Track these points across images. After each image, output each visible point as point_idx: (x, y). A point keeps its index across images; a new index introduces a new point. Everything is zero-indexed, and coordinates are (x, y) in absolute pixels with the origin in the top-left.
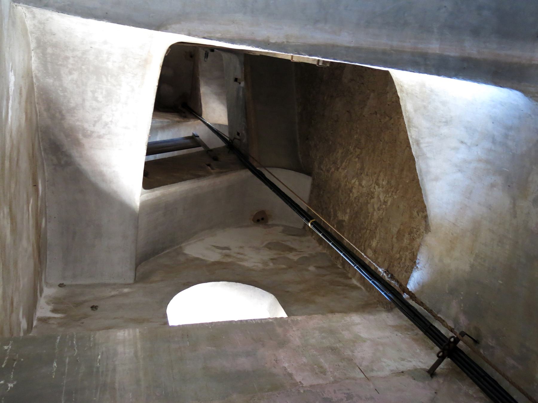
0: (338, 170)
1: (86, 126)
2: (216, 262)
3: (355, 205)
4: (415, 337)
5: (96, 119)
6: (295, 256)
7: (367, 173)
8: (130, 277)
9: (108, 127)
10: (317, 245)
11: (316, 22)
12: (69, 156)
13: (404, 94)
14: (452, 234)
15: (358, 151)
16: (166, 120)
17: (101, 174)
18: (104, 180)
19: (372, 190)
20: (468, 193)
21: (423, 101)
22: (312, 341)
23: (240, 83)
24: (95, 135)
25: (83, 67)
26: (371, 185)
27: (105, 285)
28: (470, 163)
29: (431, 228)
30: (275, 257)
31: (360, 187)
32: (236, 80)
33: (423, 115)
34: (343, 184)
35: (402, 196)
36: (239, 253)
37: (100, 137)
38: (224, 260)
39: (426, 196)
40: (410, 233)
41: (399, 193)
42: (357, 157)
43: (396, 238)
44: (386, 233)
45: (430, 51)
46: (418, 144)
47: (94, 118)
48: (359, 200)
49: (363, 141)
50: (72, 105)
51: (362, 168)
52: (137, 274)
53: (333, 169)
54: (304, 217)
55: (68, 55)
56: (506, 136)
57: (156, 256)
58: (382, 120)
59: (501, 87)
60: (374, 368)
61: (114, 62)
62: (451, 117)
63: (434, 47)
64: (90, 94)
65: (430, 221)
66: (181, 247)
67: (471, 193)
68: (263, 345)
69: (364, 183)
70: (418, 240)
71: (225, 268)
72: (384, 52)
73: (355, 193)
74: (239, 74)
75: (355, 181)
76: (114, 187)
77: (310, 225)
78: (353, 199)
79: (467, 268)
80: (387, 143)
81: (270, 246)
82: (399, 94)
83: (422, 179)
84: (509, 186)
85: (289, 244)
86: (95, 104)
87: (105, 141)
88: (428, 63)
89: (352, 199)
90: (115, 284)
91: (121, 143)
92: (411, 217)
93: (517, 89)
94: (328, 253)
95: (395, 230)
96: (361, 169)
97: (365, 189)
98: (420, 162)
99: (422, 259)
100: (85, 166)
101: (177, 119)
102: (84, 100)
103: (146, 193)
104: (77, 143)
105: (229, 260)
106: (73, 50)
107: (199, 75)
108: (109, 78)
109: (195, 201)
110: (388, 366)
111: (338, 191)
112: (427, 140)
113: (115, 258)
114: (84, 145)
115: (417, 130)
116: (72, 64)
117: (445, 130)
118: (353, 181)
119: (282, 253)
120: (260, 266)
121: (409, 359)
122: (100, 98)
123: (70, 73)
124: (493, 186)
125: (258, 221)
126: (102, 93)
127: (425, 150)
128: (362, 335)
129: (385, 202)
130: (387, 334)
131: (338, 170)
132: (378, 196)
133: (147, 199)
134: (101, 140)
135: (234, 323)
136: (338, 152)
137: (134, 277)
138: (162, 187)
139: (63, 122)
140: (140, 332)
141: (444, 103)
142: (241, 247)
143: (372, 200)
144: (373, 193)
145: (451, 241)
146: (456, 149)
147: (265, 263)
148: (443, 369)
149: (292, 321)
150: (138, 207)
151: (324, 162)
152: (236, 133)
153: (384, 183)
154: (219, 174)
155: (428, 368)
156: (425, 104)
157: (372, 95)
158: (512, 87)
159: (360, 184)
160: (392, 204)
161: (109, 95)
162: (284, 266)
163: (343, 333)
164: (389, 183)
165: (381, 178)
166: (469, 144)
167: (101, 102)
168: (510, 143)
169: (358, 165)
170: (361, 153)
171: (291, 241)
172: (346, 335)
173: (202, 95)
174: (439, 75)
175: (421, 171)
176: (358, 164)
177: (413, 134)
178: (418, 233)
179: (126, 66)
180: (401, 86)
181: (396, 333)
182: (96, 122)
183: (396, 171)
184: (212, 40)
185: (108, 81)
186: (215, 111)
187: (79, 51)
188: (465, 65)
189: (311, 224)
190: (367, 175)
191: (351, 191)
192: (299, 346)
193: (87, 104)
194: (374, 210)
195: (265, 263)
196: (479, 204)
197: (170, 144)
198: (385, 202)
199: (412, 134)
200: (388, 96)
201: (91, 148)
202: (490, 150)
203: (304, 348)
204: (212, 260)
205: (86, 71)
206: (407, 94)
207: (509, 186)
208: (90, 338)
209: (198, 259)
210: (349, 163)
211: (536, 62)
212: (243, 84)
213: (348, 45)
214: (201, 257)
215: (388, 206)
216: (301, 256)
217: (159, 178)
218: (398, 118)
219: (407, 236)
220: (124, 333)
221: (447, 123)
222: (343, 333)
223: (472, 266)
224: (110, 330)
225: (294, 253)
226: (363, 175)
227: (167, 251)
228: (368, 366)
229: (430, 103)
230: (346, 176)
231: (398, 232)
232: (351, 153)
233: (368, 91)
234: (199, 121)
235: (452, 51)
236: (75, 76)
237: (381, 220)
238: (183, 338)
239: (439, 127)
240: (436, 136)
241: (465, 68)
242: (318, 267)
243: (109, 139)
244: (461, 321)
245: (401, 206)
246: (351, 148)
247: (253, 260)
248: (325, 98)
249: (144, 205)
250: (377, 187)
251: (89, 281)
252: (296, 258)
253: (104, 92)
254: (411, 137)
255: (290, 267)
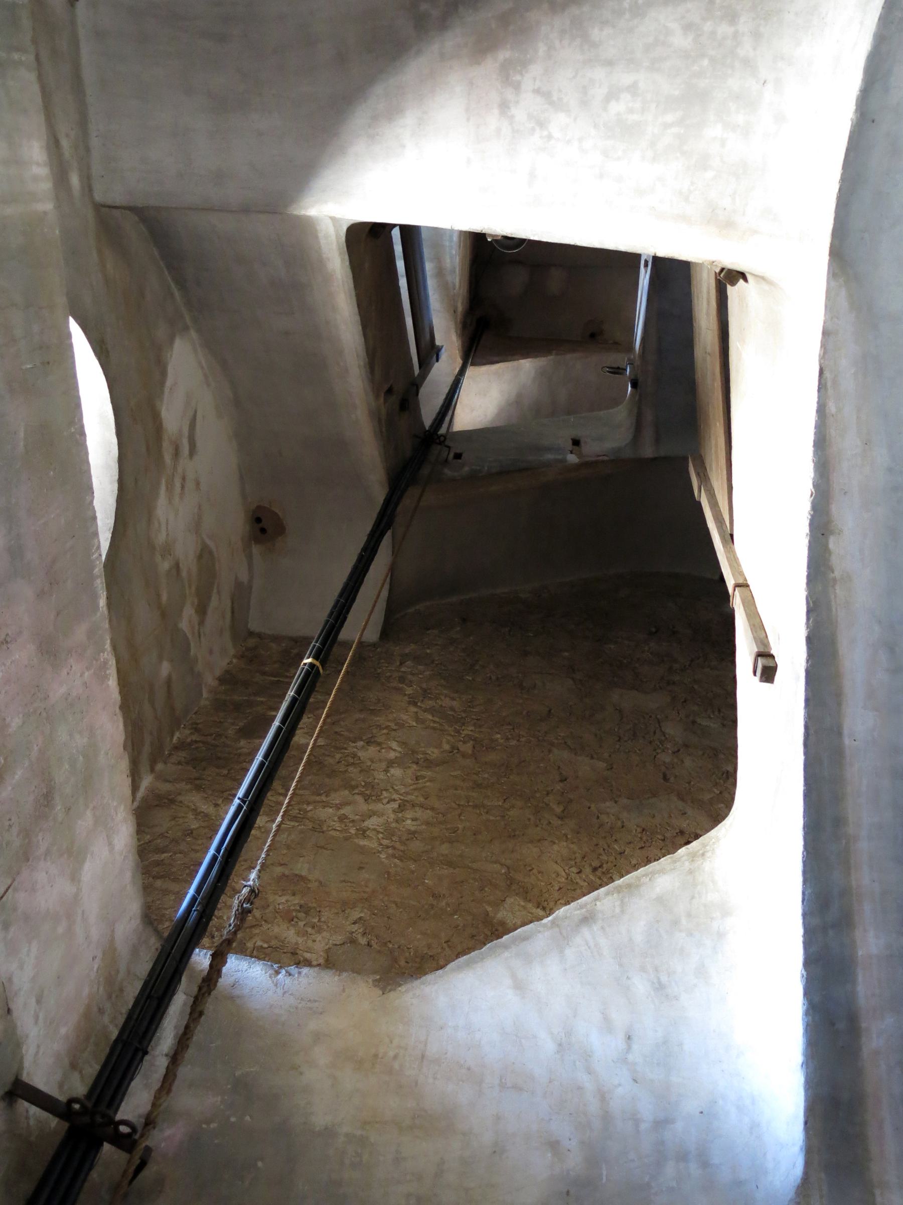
0: (409, 703)
1: (535, 69)
2: (161, 424)
3: (338, 756)
4: (95, 1009)
5: (555, 98)
6: (190, 622)
7: (423, 777)
8: (112, 192)
9: (533, 130)
10: (218, 673)
11: (891, 649)
12: (443, 24)
13: (687, 864)
14: (396, 1057)
15: (467, 748)
16: (457, 281)
17: (393, 113)
18: (375, 118)
19: (385, 794)
20: (514, 1082)
21: (689, 915)
22: (62, 734)
23: (571, 452)
24: (509, 94)
25: (706, 62)
26: (397, 791)
27: (83, 123)
28: (589, 1071)
29: (392, 995)
30: (184, 574)
31: (384, 765)
32: (576, 442)
33: (658, 922)
34: (381, 720)
35: (388, 873)
36: (184, 479)
37: (504, 106)
38: (166, 444)
39: (468, 964)
40: (305, 909)
41: (396, 866)
42: (453, 748)
43: (284, 875)
44: (288, 847)
45: (858, 934)
46: (587, 919)
47: (560, 91)
48: (353, 764)
49: (492, 757)
50: (596, 33)
51: (429, 764)
52: (114, 211)
53: (409, 691)
54: (323, 644)
55: (742, 19)
56: (682, 1157)
57: (162, 264)
58: (551, 797)
59: (806, 1123)
60: (12, 929)
61: (723, 143)
62: (676, 998)
63: (870, 942)
64: (627, 79)
65: (409, 986)
66: (186, 328)
67: (517, 1088)
68: (41, 595)
69: (396, 772)
70: (292, 932)
71: (148, 449)
72: (839, 822)
73: (367, 754)
74: (592, 449)
75: (395, 750)
76: (359, 147)
77: (308, 661)
78: (351, 750)
79: (320, 1120)
80: (503, 817)
81: (205, 555)
82: (682, 851)
83: (506, 947)
84: (568, 1193)
85: (214, 602)
86: (599, 92)
87: (493, 120)
88: (831, 933)
89: (351, 747)
90: (88, 150)
91: (449, 163)
92: (345, 906)
93: (808, 1164)
94: (203, 703)
95: (301, 867)
96: (426, 760)
97: (382, 776)
98: (547, 934)
99: (304, 982)
100: (414, 69)
101: (460, 308)
102: (610, 63)
103: (337, 231)
104: (483, 46)
105: (168, 458)
106: (757, 36)
107: (557, 354)
108: (675, 130)
109: (311, 360)
110: (21, 967)
111: (361, 711)
112: (602, 941)
113: (165, 152)
114: (479, 64)
115: (618, 910)
116: (713, 33)
117: (640, 986)
118: (394, 745)
119: (193, 588)
120: (161, 538)
121: (41, 1016)
122: (615, 108)
123: (688, 27)
124: (554, 1145)
125: (258, 520)
126: (631, 111)
127: (578, 940)
128: (87, 866)
129: (363, 833)
130: (95, 933)
131: (409, 703)
132: (372, 814)
133: (321, 235)
134: (496, 111)
135: (88, 498)
136: (453, 699)
137: (109, 202)
138: (351, 276)
139: (545, 6)
140: (45, 213)
141: (701, 971)
142: (198, 484)
143: (359, 799)
144: (379, 800)
145: (376, 1056)
146: (607, 1025)
147: (167, 550)
148: (27, 1118)
149: (106, 663)
150: (303, 212)
151: (421, 667)
152: (458, 451)
153: (409, 822)
154: (375, 415)
155: (25, 1078)
156: (684, 921)
157: (602, 765)
158: (809, 1151)
159: (391, 763)
160: (362, 850)
161: (625, 130)
162: (164, 598)
163: (89, 813)
164: (413, 834)
165: (419, 813)
166: (630, 1057)
167: (605, 109)
168: (670, 1170)
169: (434, 753)
170: (464, 756)
171: (220, 603)
172: (85, 823)
173: (515, 363)
174: (807, 963)
175: (525, 938)
176: (436, 751)
177: (605, 901)
178: (310, 930)
179: (710, 174)
180: (703, 855)
181: (100, 955)
182: (546, 95)
183: (445, 849)
184: (819, 390)
185: (666, 126)
186: (484, 397)
187: (755, 49)
188: (841, 1025)
189: (311, 665)
190: (417, 778)
191: (369, 743)
192: (47, 698)
193: (599, 73)
194: (338, 807)
195: (167, 550)
196: (498, 1118)
197: (422, 293)
198: (363, 833)
199: (603, 900)
200: (608, 804)
201: (471, 84)
202: (637, 1121)
203: (44, 714)
204: (164, 414)
205: (696, 68)
206: (691, 872)
207: (568, 1193)
208: (17, 49)
209: (164, 374)
210: (434, 728)
211: (879, 1199)
212: (572, 459)
213: (846, 731)
214: (169, 383)
215: (356, 840)
216: (190, 637)
217: (367, 265)
218: (566, 835)
219: (296, 900)
220: (38, 164)
221: (659, 987)
222: (89, 813)
223: (329, 1133)
224: (42, 118)
225: (195, 619)
226: (415, 766)
227: (177, 294)
228: (15, 909)
229: (690, 934)
230: (401, 725)
231: (302, 878)
232: (458, 732)
233: (606, 755)
234: (459, 362)
235: (867, 987)
236: (681, 41)
237: (318, 827)
238: (41, 348)
239: (643, 969)
240: (621, 965)
241: (833, 1024)
242: (169, 681)
243: (498, 131)
244: (168, 1132)
245: (364, 875)
246: (468, 730)
247: (171, 518)
248: (566, 654)
249: (307, 226)
250: (395, 805)
251: (89, 74)
252: (184, 625)
253: (635, 117)
254: (597, 899)
255: (164, 615)
